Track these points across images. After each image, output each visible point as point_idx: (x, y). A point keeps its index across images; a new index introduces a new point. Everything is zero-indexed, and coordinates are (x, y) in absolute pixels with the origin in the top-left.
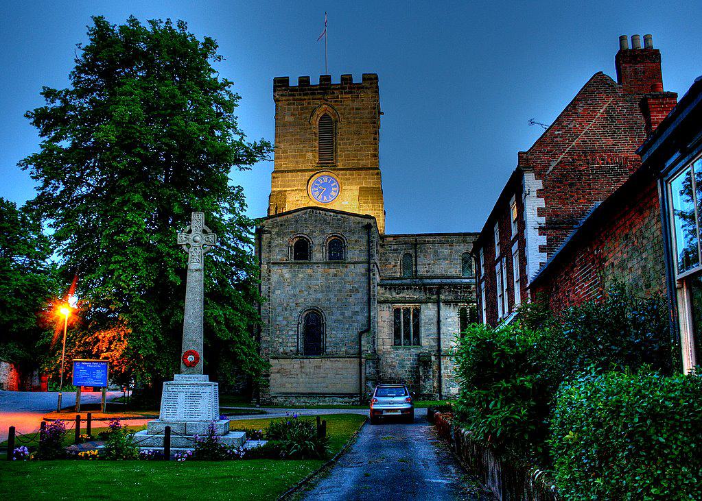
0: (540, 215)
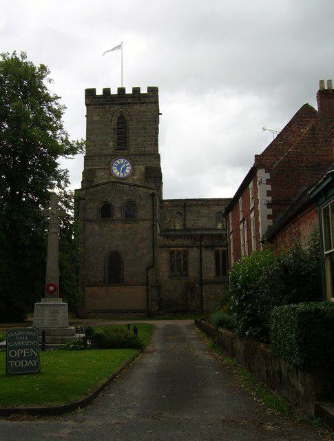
0: (268, 196)
